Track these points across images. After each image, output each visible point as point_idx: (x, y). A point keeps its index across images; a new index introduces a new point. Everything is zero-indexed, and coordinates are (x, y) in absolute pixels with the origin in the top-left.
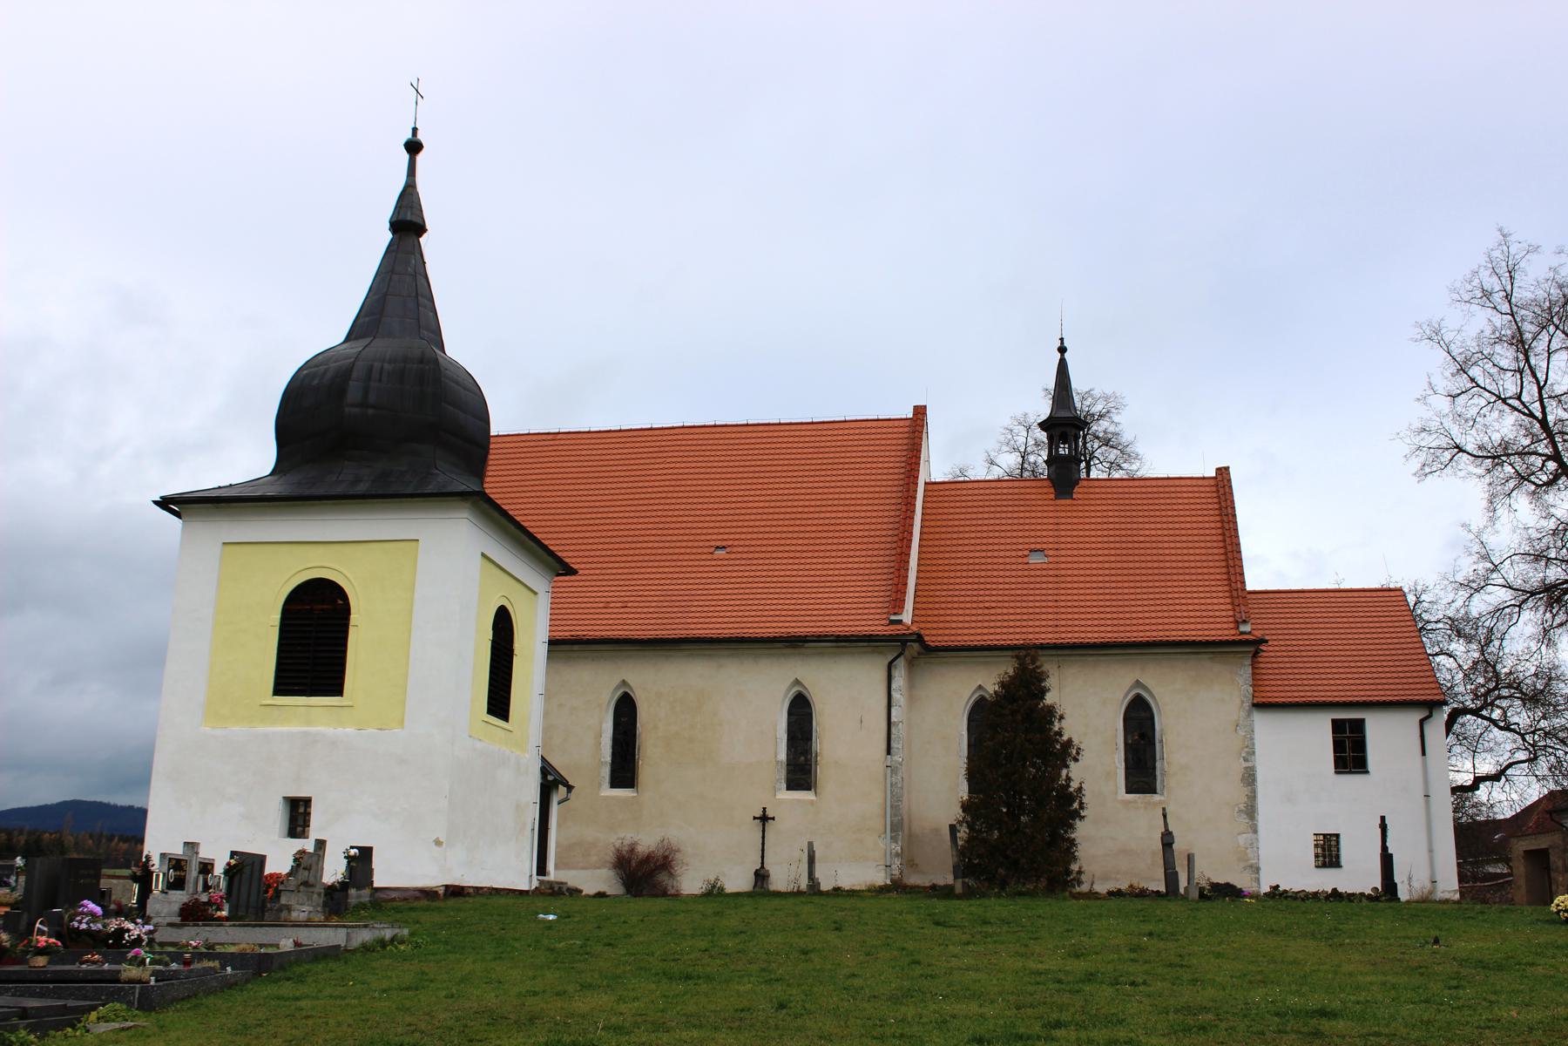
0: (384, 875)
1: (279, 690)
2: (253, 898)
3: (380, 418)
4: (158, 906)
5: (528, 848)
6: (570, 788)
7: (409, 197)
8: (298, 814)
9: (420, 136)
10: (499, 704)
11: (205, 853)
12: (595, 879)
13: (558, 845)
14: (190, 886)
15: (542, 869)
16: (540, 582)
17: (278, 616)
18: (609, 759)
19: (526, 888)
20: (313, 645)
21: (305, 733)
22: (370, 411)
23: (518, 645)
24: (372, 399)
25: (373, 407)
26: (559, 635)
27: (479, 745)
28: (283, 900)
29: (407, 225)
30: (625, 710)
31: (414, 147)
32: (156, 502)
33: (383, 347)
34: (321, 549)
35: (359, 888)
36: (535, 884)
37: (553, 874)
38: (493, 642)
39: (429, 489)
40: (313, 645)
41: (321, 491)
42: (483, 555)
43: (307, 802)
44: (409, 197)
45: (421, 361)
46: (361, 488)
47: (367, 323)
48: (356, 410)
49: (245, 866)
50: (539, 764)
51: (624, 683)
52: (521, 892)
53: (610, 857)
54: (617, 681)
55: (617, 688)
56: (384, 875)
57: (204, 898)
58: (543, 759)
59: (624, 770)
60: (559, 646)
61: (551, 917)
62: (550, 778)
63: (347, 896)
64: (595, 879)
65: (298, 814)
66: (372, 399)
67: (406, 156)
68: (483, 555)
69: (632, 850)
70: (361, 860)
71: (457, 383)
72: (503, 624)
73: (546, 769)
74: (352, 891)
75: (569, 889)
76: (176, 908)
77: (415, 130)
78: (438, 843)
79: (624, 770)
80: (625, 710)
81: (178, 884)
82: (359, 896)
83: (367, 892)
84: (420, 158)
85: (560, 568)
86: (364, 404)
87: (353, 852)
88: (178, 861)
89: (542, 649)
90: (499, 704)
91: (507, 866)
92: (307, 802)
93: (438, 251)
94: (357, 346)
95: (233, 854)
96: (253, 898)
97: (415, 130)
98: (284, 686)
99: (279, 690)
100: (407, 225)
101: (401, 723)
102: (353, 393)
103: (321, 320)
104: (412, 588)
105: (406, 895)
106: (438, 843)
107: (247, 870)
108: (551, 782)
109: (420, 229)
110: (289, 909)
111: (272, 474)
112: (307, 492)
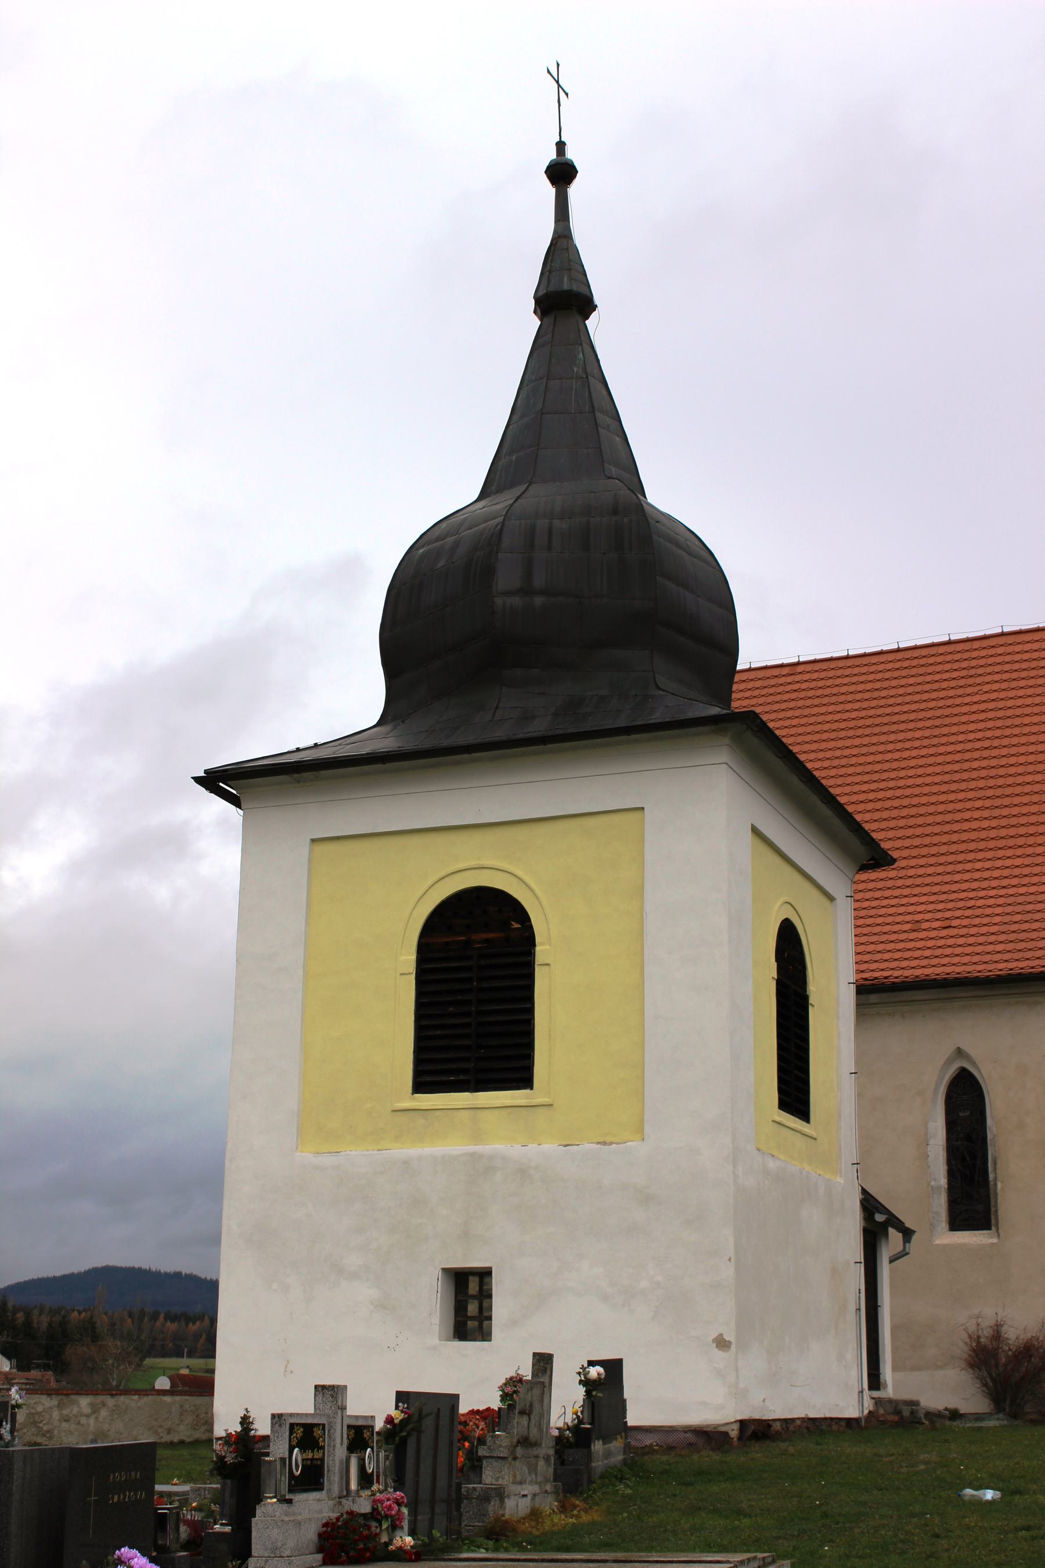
0: (645, 1406)
1: (422, 1084)
2: (442, 1482)
3: (550, 612)
4: (275, 1533)
5: (853, 1344)
6: (907, 1234)
7: (562, 255)
8: (470, 1302)
9: (570, 154)
10: (794, 1094)
11: (356, 1407)
12: (946, 1388)
13: (894, 1329)
14: (332, 1479)
15: (875, 1380)
16: (835, 878)
17: (412, 957)
18: (943, 1181)
19: (852, 1412)
20: (474, 1001)
21: (473, 1155)
22: (538, 601)
23: (814, 988)
24: (539, 581)
25: (543, 592)
26: (881, 972)
27: (772, 1164)
28: (489, 1476)
29: (563, 298)
30: (965, 1098)
31: (561, 173)
32: (198, 780)
33: (541, 496)
34: (477, 838)
35: (606, 1439)
36: (868, 1405)
37: (890, 1391)
38: (780, 983)
39: (657, 717)
40: (474, 1001)
41: (470, 739)
42: (755, 831)
43: (485, 1274)
44: (562, 255)
45: (615, 511)
46: (538, 727)
47: (514, 463)
48: (516, 601)
49: (425, 1416)
50: (857, 1197)
51: (960, 1052)
52: (849, 1421)
53: (961, 1349)
54: (946, 1050)
55: (949, 1062)
56: (645, 1406)
57: (364, 1506)
58: (864, 1191)
59: (971, 1197)
60: (874, 994)
61: (989, 1495)
62: (880, 1218)
63: (589, 1457)
64: (946, 1388)
65: (470, 1302)
66: (539, 581)
67: (551, 191)
68: (755, 831)
69: (997, 1335)
70: (606, 1384)
71: (678, 545)
72: (789, 945)
73: (869, 1205)
74: (598, 1446)
75: (928, 1414)
76: (311, 1533)
77: (561, 146)
78: (722, 1343)
79: (971, 1197)
80: (965, 1098)
81: (311, 1478)
82: (608, 1454)
83: (617, 1444)
84: (574, 191)
85: (869, 856)
86: (526, 590)
87: (594, 1372)
88: (309, 1428)
89: (848, 996)
90: (794, 1094)
91: (824, 1384)
92: (485, 1274)
93: (611, 334)
94: (501, 503)
95: (402, 1397)
96: (442, 1482)
97: (561, 146)
98: (430, 1076)
99: (422, 1084)
100: (563, 298)
101: (639, 1130)
102: (507, 577)
103: (441, 465)
104: (639, 891)
105: (671, 1439)
106: (722, 1343)
107: (428, 1423)
108: (878, 1223)
109: (585, 305)
110: (500, 1494)
111: (379, 724)
112: (447, 742)
